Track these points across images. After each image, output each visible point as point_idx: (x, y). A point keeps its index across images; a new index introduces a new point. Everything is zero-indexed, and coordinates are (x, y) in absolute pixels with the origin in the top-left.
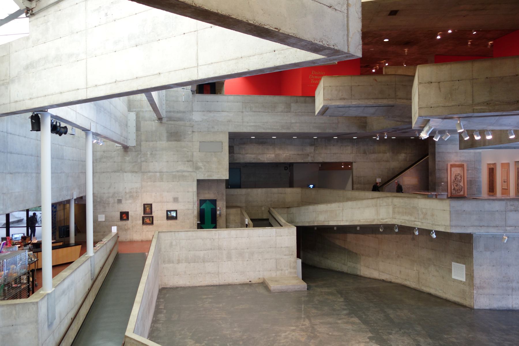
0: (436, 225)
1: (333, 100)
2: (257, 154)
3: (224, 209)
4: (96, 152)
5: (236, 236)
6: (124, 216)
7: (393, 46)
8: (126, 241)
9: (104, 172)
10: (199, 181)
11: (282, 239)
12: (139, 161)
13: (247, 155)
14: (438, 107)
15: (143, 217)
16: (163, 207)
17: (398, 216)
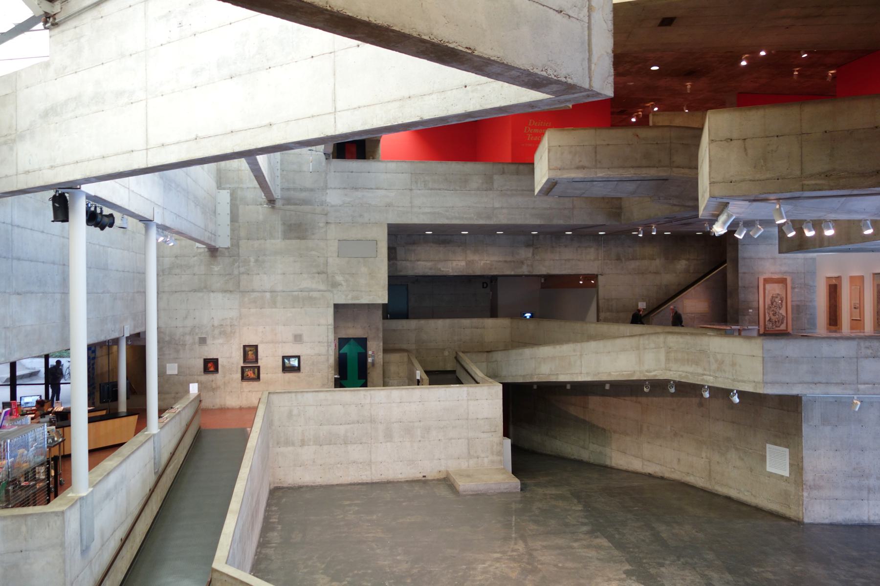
0: (739, 381)
1: (564, 169)
2: (435, 261)
3: (379, 353)
4: (163, 257)
5: (401, 400)
6: (210, 365)
7: (666, 78)
8: (214, 408)
9: (176, 292)
10: (337, 307)
11: (479, 404)
12: (236, 272)
13: (419, 263)
14: (743, 181)
15: (242, 368)
16: (276, 351)
17: (674, 366)
